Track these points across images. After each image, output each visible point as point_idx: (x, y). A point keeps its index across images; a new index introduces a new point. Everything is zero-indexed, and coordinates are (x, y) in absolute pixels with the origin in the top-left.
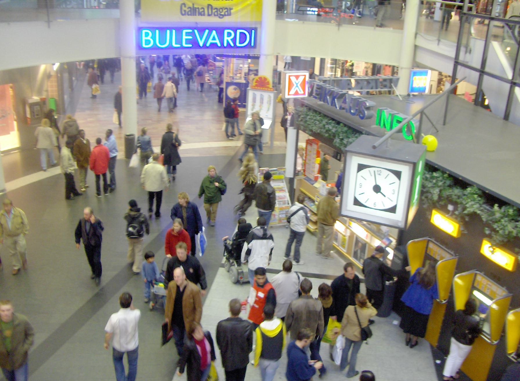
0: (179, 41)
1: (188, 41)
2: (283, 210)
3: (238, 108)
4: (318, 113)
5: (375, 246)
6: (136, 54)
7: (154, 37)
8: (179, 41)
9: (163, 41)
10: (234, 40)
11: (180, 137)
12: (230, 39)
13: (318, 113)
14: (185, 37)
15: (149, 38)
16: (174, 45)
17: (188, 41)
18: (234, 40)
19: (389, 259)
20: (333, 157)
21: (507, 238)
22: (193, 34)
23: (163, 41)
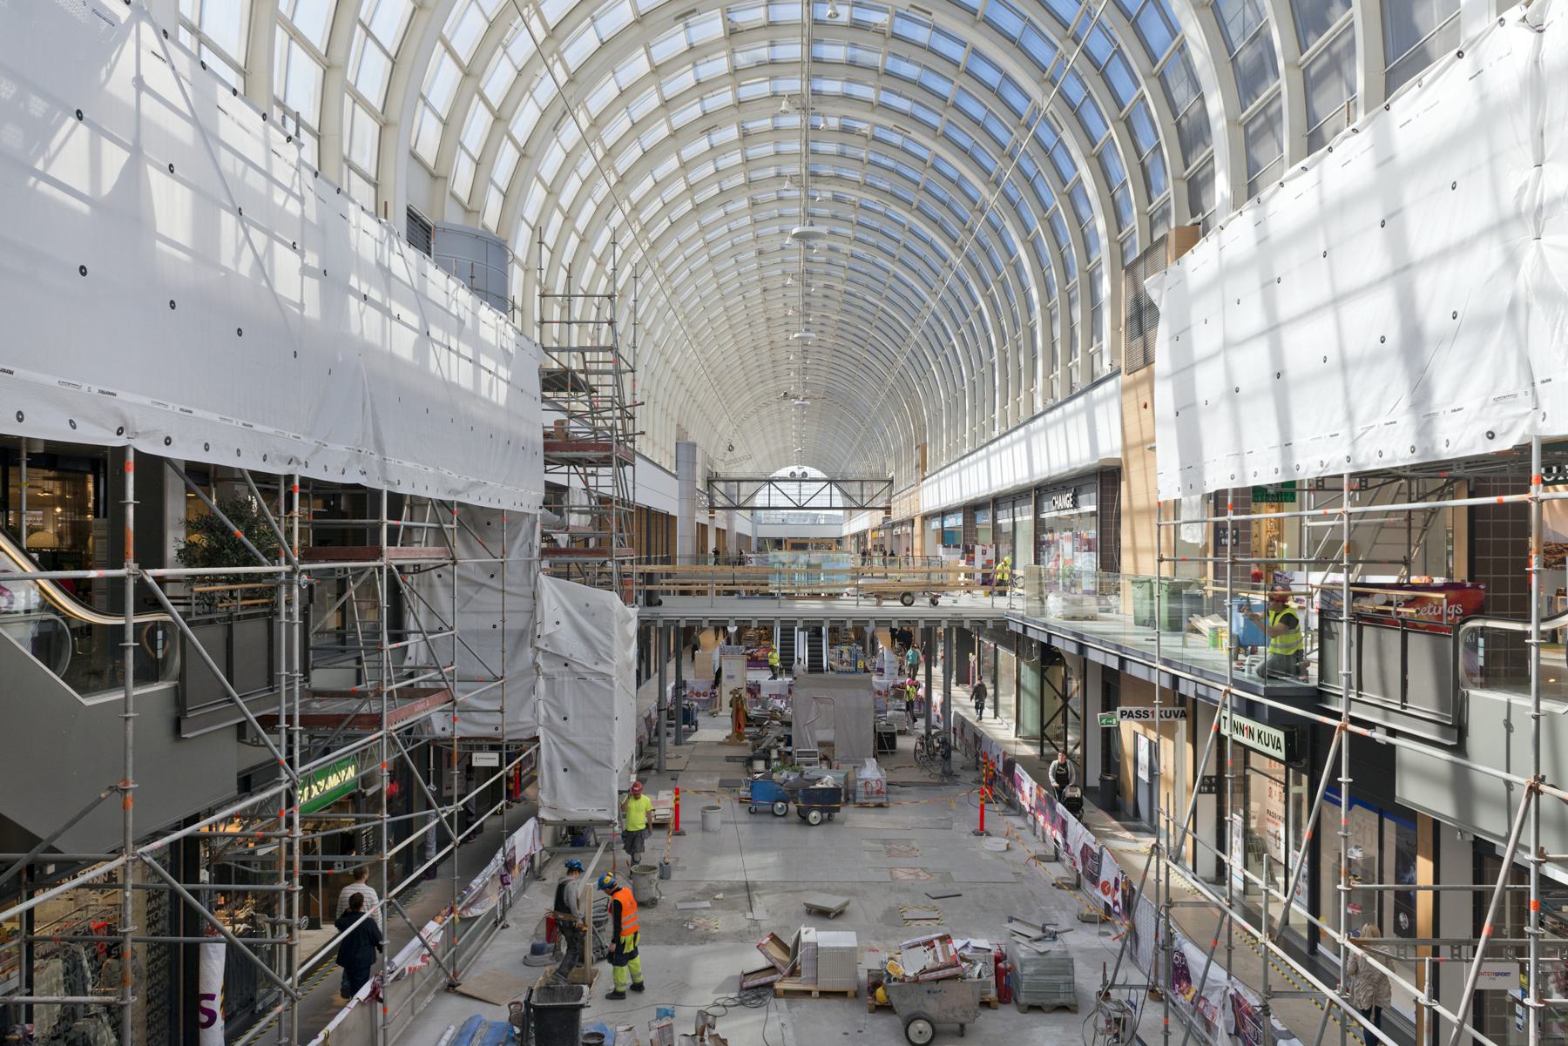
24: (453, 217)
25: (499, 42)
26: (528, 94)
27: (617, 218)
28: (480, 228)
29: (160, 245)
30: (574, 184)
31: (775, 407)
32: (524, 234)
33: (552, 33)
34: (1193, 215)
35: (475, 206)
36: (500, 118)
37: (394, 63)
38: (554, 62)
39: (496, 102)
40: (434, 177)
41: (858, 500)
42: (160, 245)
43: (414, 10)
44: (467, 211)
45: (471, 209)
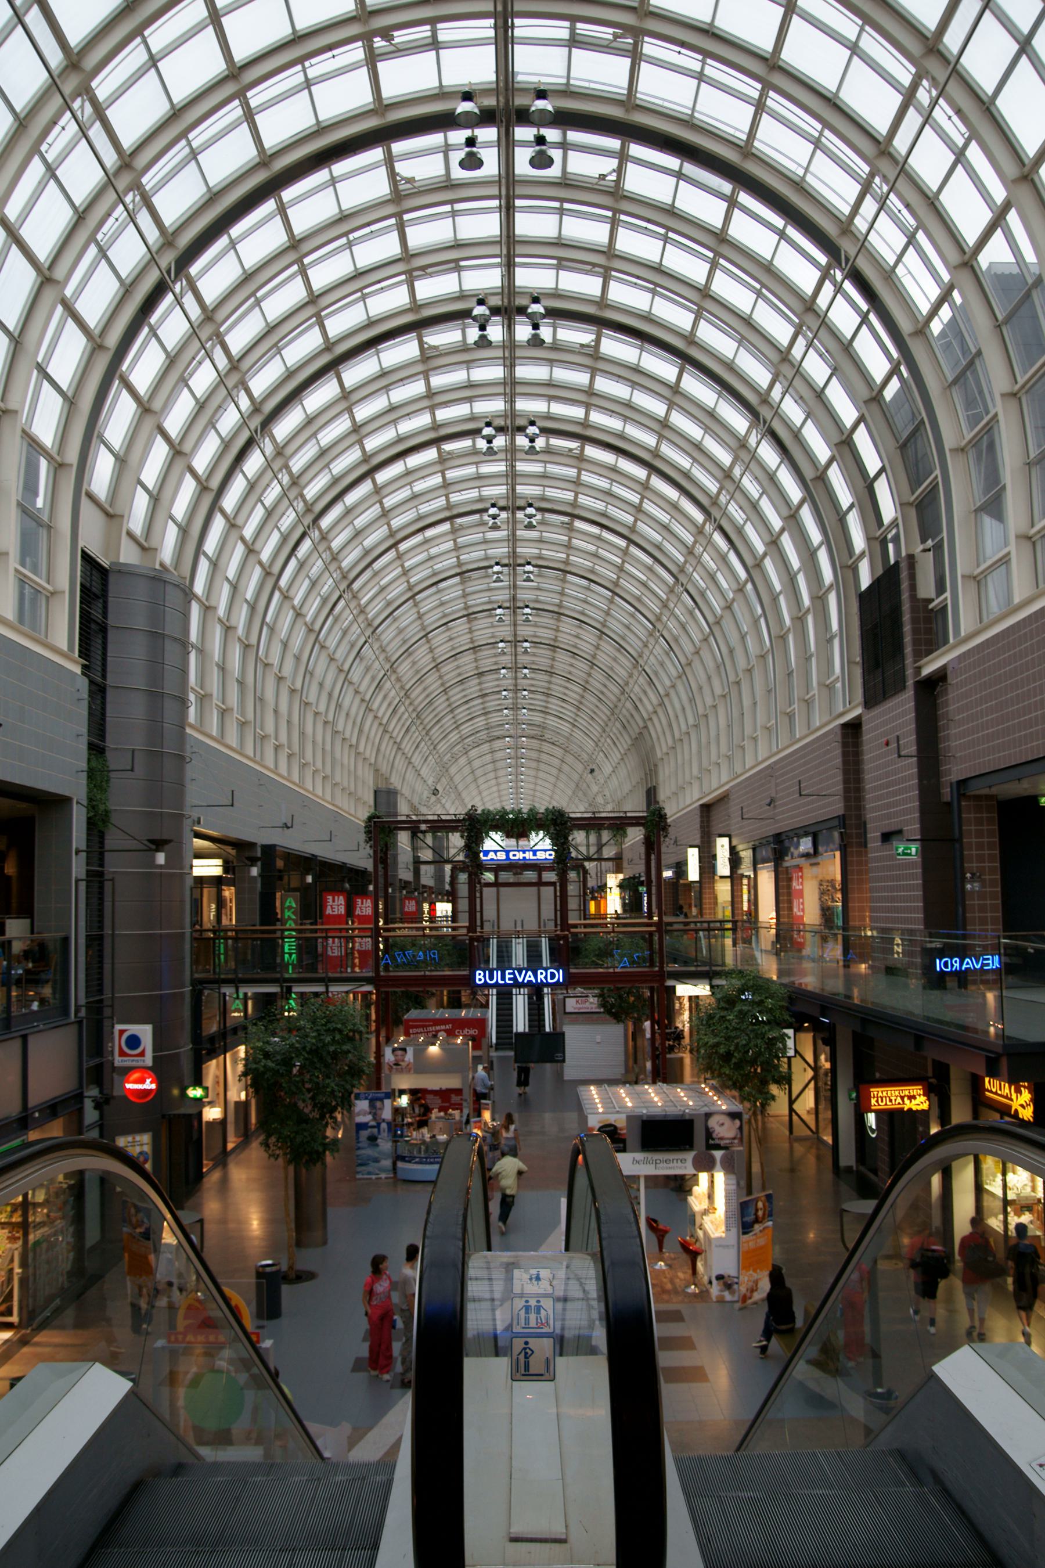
0: (503, 978)
1: (510, 979)
2: (328, 747)
3: (256, 1243)
4: (951, 983)
5: (158, 239)
6: (985, 495)
7: (485, 976)
8: (503, 978)
9: (491, 978)
10: (546, 977)
11: (362, 837)
12: (542, 977)
13: (951, 983)
14: (508, 976)
15: (481, 977)
16: (500, 982)
17: (510, 979)
18: (546, 977)
19: (273, 439)
20: (697, 997)
21: (331, 1117)
22: (513, 973)
23: (491, 978)
24: (128, 555)
25: (92, 239)
26: (92, 251)
27: (254, 463)
28: (157, 567)
29: (987, 1093)
30: (238, 486)
31: (492, 775)
32: (141, 502)
33: (235, 364)
34: (923, 541)
35: (117, 510)
36: (178, 452)
37: (17, 342)
38: (213, 347)
39: (43, 252)
40: (109, 516)
41: (583, 849)
42: (987, 1093)
43: (42, 284)
44: (143, 548)
45: (146, 548)
